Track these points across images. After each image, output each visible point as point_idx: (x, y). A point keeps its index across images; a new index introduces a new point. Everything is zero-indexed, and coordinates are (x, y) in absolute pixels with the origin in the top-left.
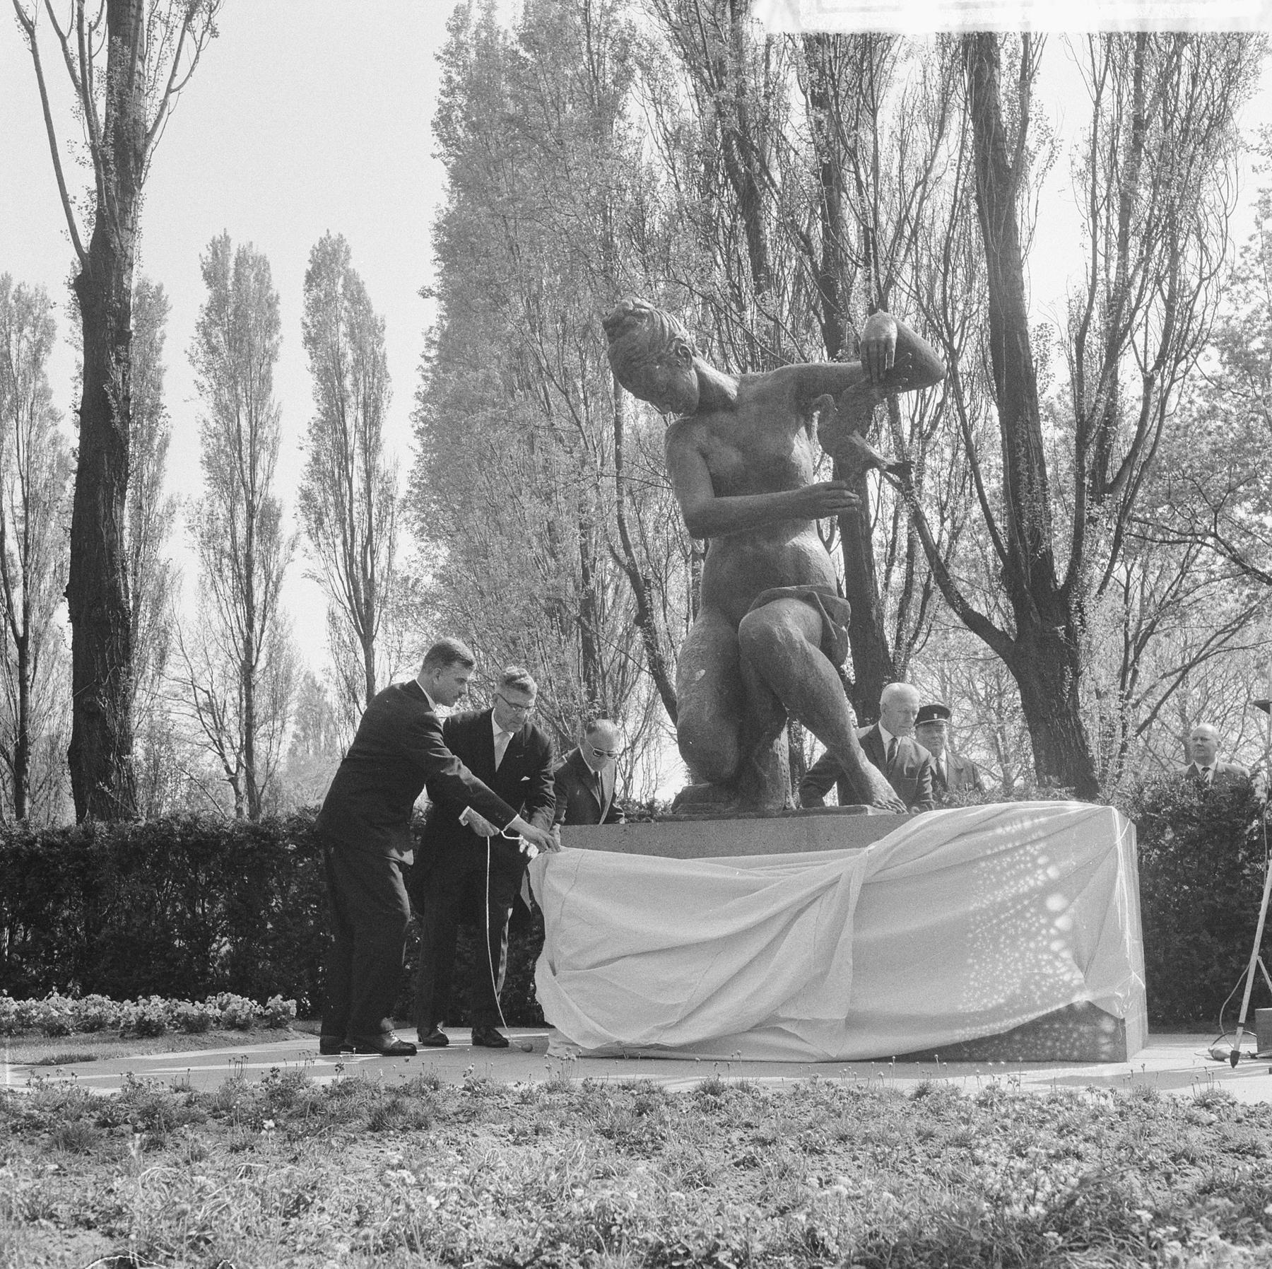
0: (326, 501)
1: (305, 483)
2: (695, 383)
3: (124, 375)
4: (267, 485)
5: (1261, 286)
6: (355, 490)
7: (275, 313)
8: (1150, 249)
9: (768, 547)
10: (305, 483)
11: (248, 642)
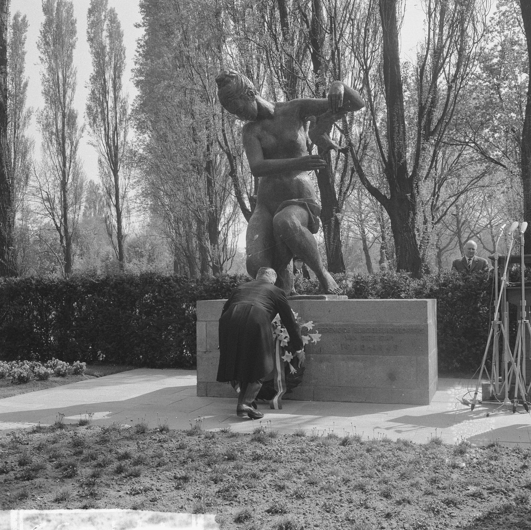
0: (97, 111)
1: (88, 103)
2: (256, 107)
3: (4, 79)
4: (71, 104)
5: (498, 35)
6: (109, 106)
7: (75, 27)
8: (453, 32)
9: (286, 180)
10: (88, 103)
11: (64, 173)
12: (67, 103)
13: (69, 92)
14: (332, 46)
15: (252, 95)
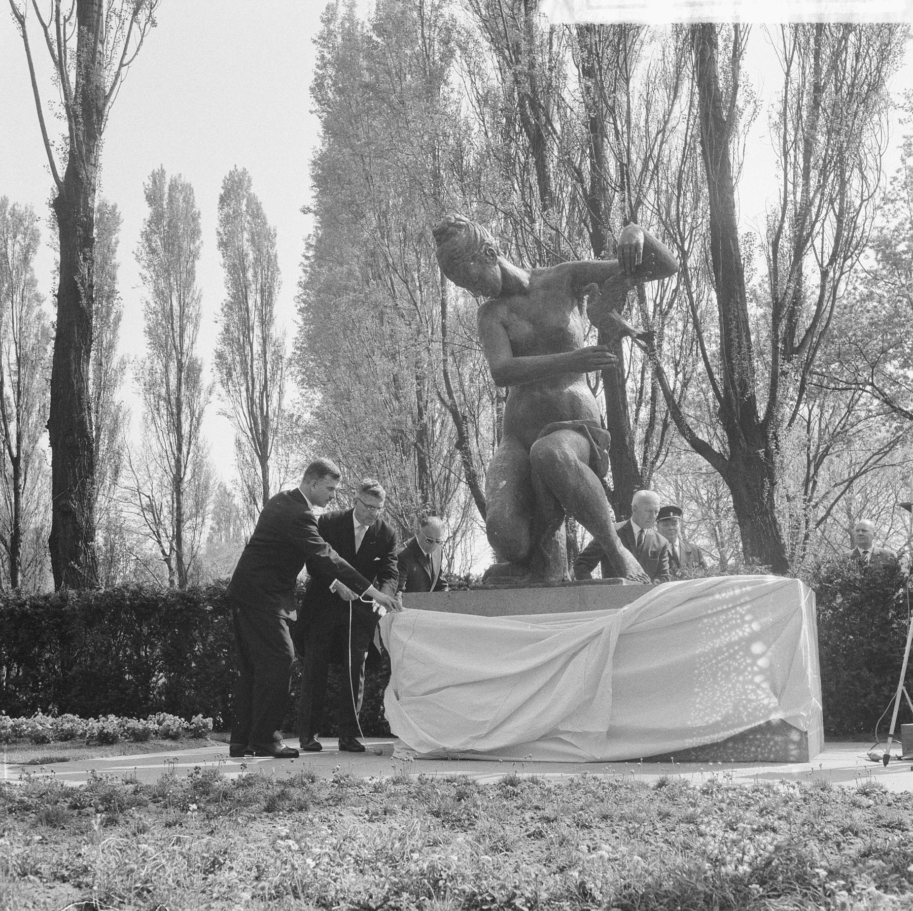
0: (234, 359)
1: (219, 347)
2: (499, 275)
3: (89, 269)
4: (192, 348)
5: (905, 205)
6: (254, 352)
7: (198, 225)
8: (826, 179)
9: (551, 393)
10: (219, 347)
11: (178, 461)
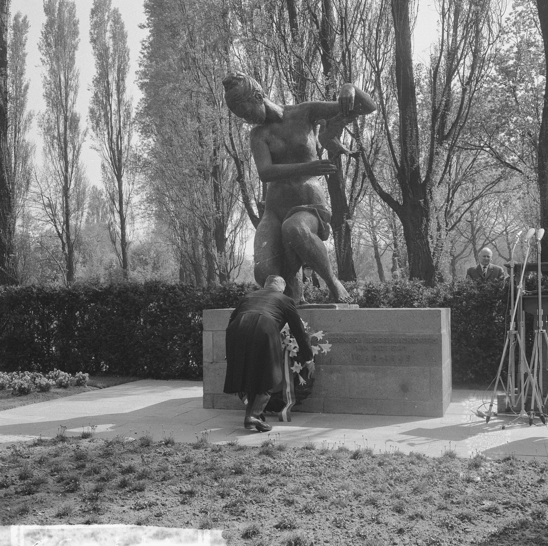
0: (100, 114)
1: (91, 106)
2: (264, 111)
3: (4, 81)
4: (73, 107)
5: (514, 36)
6: (113, 109)
7: (77, 28)
8: (468, 33)
9: (295, 185)
10: (91, 106)
11: (66, 178)
12: (69, 106)
13: (71, 94)
14: (342, 48)
15: (261, 98)
